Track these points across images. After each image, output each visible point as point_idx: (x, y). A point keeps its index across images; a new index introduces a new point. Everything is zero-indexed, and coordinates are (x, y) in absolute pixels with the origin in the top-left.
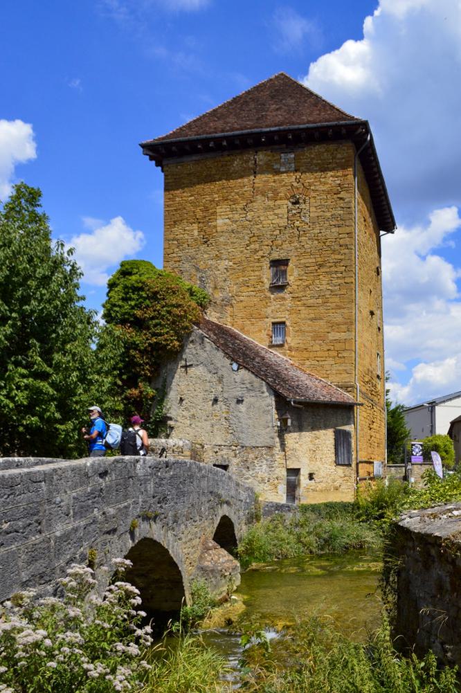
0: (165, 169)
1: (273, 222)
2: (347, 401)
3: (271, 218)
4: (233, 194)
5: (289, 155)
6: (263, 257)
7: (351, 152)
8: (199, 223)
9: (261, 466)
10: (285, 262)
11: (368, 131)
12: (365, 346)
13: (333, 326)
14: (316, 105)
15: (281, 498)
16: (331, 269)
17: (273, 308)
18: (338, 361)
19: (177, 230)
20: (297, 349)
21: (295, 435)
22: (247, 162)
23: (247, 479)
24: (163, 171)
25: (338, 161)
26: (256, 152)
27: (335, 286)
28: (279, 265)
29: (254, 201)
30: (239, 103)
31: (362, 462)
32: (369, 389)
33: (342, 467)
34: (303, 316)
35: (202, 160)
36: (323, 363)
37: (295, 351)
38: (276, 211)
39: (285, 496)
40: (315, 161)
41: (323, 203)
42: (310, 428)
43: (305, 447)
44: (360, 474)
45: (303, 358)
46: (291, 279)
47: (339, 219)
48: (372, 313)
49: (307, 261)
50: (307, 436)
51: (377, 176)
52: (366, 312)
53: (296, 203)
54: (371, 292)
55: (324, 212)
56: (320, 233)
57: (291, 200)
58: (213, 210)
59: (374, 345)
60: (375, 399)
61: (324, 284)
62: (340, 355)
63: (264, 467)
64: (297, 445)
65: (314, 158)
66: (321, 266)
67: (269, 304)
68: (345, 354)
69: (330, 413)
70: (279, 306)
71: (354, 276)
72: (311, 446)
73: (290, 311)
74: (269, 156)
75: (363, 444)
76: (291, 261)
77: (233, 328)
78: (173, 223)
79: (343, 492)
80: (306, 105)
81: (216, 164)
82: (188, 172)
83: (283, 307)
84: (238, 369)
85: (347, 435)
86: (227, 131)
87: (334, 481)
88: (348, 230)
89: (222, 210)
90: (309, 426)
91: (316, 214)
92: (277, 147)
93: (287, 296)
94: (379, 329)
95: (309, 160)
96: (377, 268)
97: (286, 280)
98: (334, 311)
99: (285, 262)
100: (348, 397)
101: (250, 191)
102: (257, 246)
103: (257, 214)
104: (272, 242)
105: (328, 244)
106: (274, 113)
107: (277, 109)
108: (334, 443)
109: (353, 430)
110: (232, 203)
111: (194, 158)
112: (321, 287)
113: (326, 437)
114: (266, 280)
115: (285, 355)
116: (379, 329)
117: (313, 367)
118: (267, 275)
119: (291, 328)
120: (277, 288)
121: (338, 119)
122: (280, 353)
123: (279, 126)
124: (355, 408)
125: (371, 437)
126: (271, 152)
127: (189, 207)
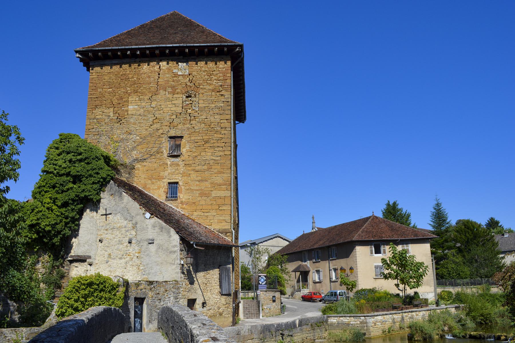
1: (172, 109)
6: (162, 134)
9: (169, 298)
17: (170, 171)
29: (158, 94)
36: (207, 214)
38: (173, 102)
46: (184, 150)
49: (196, 138)
51: (242, 82)
57: (186, 95)
62: (220, 208)
63: (172, 298)
66: (206, 142)
73: (183, 174)
79: (225, 317)
87: (219, 308)
91: (204, 105)
92: (176, 57)
98: (216, 175)
110: (140, 95)
114: (165, 151)
118: (166, 147)
119: (183, 187)
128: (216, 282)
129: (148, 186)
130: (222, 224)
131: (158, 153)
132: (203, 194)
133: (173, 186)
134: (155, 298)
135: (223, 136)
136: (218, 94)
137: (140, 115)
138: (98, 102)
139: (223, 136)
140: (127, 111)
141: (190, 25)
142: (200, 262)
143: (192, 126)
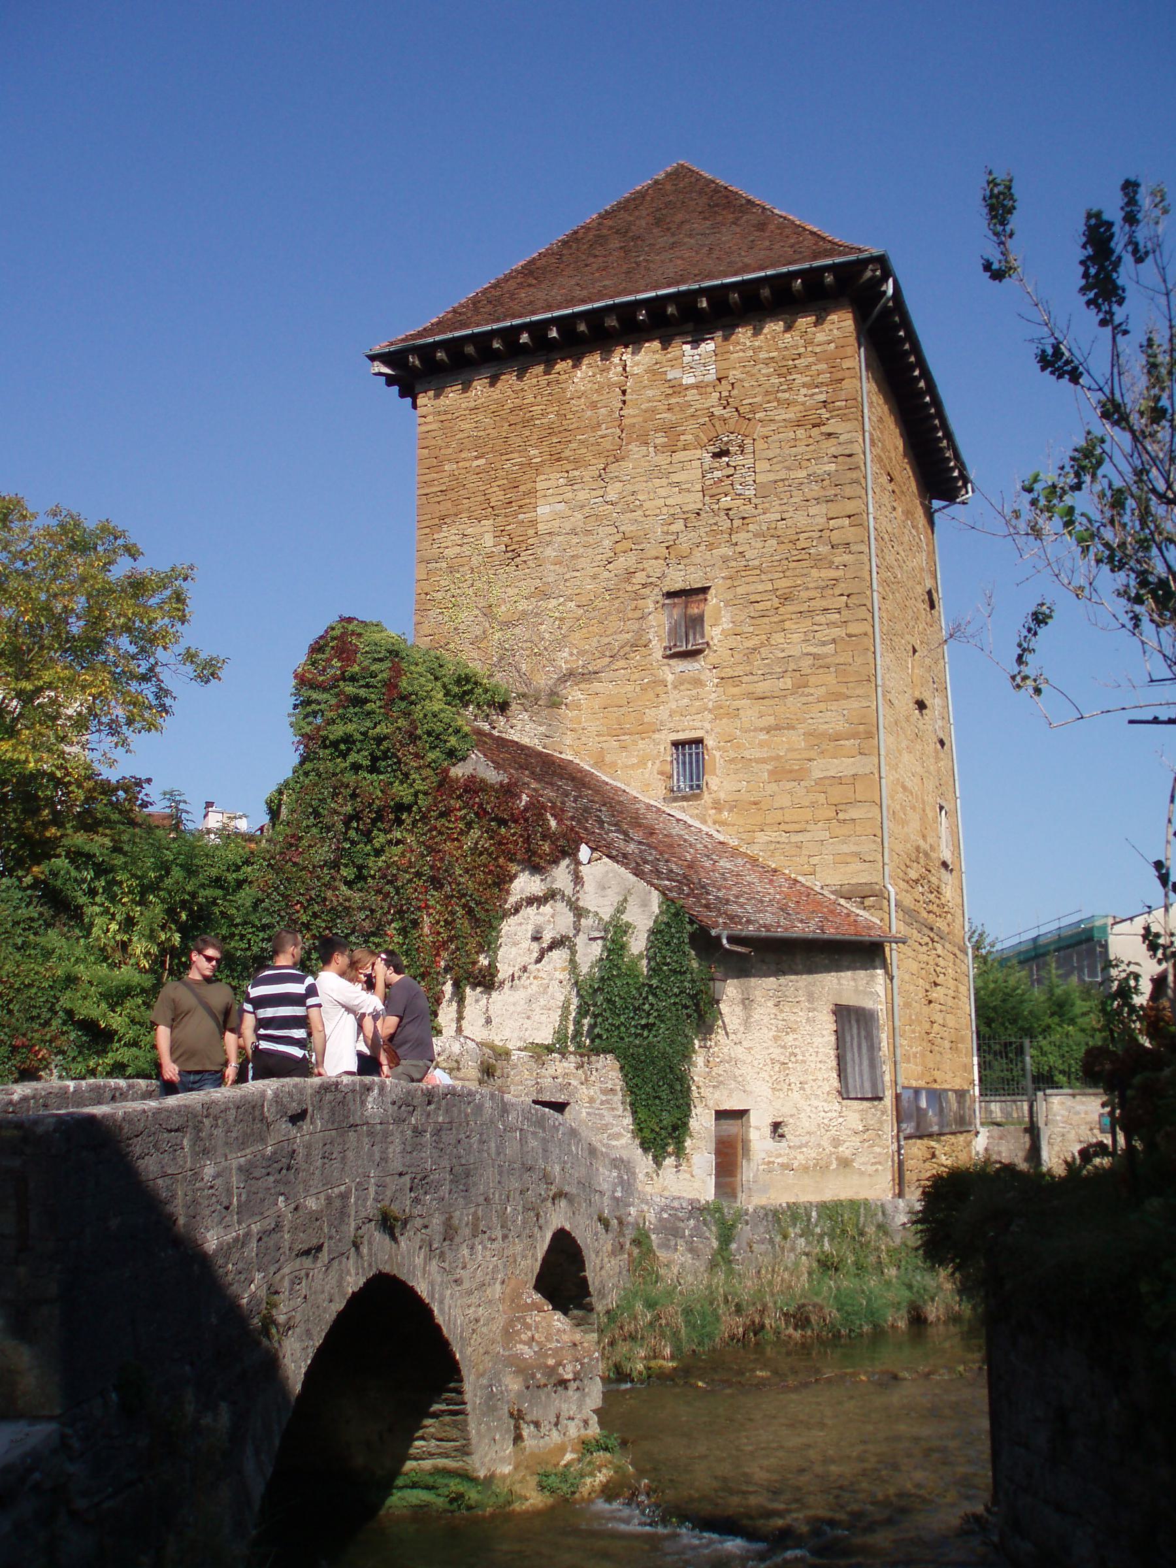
1: (670, 501)
3: (662, 492)
4: (573, 445)
6: (644, 586)
12: (905, 788)
14: (761, 227)
25: (818, 350)
27: (824, 644)
30: (578, 247)
32: (921, 898)
38: (675, 478)
40: (763, 355)
46: (714, 633)
49: (751, 588)
54: (915, 651)
58: (530, 485)
61: (793, 641)
62: (841, 816)
64: (739, 1049)
66: (786, 599)
68: (854, 813)
72: (776, 1052)
73: (720, 712)
77: (577, 761)
79: (862, 1173)
82: (472, 404)
88: (851, 507)
91: (772, 477)
97: (703, 637)
98: (822, 706)
104: (667, 548)
107: (673, 246)
118: (659, 624)
119: (717, 754)
124: (887, 949)
129: (608, 758)
135: (840, 573)
136: (815, 432)
140: (533, 523)
141: (722, 203)
143: (739, 549)
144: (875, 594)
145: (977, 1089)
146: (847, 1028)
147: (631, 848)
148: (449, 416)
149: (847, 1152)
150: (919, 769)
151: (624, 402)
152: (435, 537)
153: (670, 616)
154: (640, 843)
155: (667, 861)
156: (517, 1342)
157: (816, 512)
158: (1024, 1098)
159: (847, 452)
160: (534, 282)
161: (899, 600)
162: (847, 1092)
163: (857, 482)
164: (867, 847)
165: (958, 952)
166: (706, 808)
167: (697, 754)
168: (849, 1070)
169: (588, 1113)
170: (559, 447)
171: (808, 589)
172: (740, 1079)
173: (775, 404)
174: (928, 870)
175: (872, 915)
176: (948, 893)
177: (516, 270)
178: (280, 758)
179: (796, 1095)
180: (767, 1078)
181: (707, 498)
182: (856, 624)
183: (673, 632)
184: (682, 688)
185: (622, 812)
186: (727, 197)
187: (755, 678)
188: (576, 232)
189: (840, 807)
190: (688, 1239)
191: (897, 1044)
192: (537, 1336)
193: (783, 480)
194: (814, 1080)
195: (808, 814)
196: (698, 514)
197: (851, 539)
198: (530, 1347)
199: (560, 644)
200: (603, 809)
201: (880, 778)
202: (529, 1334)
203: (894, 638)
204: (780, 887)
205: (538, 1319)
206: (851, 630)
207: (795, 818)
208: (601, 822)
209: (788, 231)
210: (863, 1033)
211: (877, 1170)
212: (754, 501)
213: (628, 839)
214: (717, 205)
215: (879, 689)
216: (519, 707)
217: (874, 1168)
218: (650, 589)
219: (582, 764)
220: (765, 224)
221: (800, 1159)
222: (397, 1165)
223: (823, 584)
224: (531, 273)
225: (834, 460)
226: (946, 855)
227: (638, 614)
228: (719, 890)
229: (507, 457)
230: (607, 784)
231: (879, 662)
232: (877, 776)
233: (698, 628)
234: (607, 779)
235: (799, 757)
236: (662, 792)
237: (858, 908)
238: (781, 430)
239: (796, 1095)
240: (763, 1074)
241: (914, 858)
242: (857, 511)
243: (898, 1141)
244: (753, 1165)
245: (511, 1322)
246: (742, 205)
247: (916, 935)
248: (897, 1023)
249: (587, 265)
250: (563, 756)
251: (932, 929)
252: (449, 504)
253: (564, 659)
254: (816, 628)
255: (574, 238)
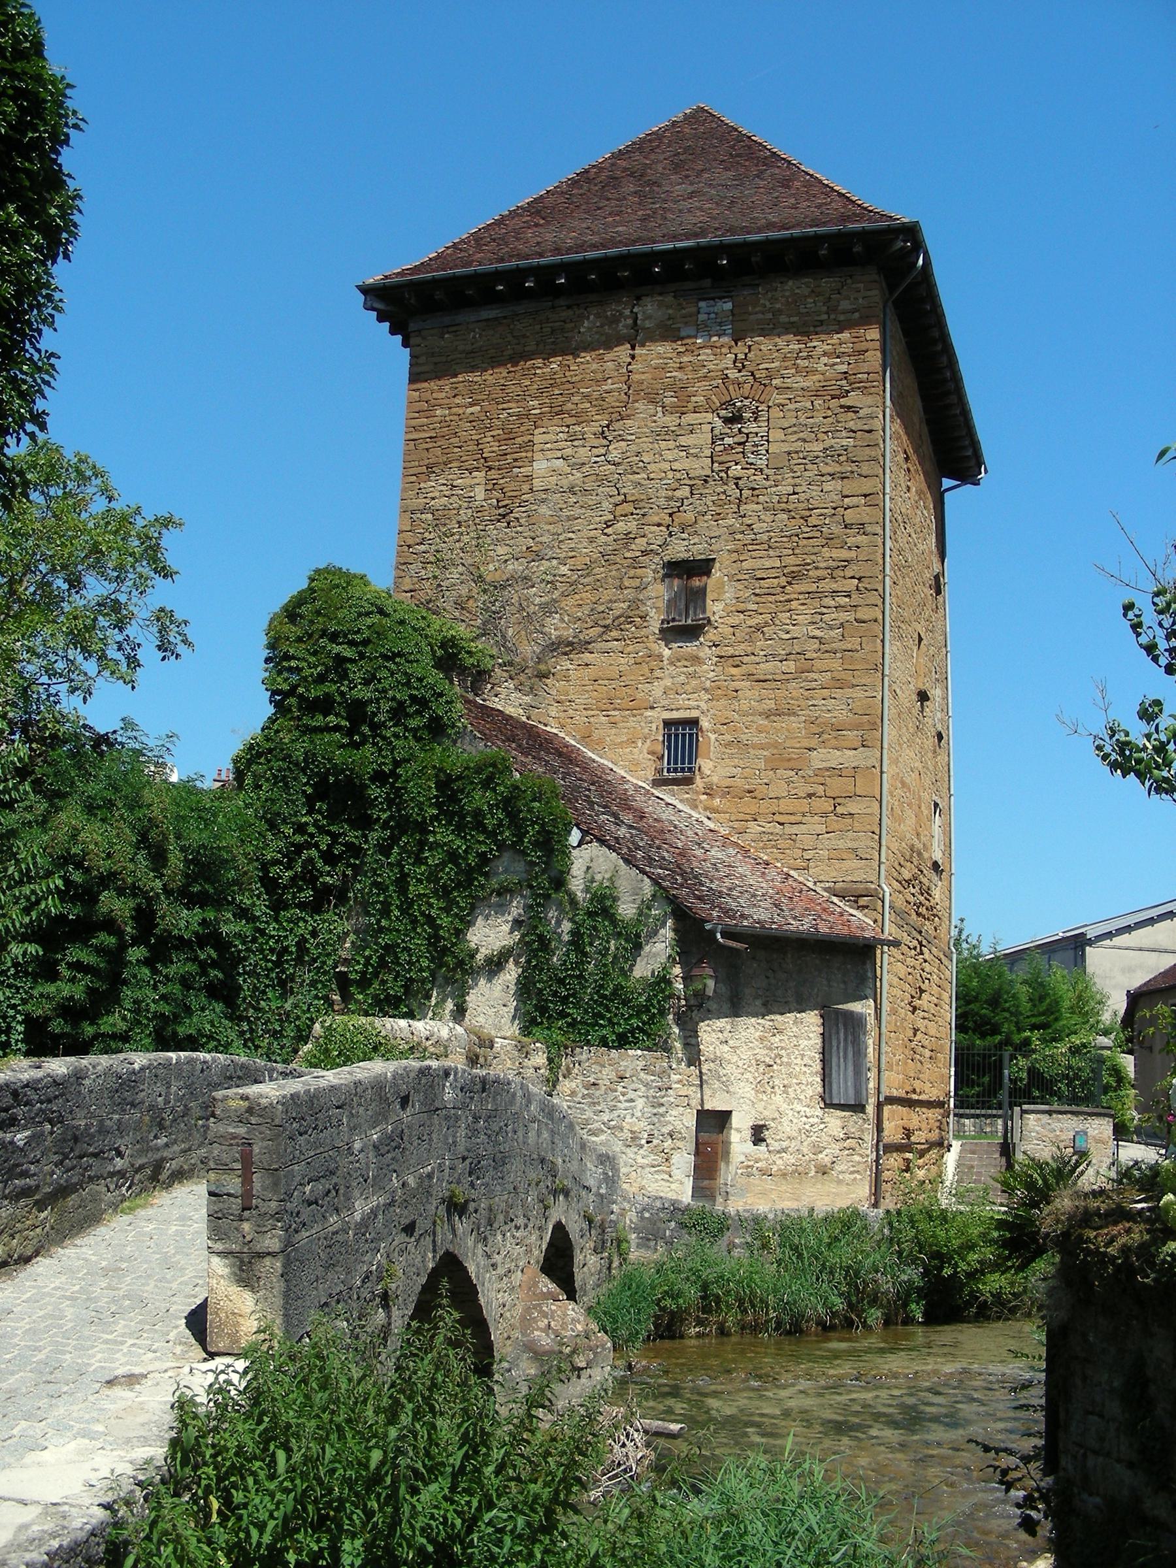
0: (413, 341)
1: (676, 466)
2: (859, 933)
3: (669, 456)
4: (576, 399)
5: (720, 303)
6: (645, 553)
7: (875, 294)
8: (490, 468)
9: (632, 1100)
10: (703, 567)
11: (918, 245)
12: (903, 784)
13: (826, 732)
14: (786, 183)
15: (679, 1186)
16: (822, 584)
17: (668, 682)
18: (835, 826)
19: (434, 486)
20: (727, 792)
21: (722, 1023)
22: (615, 320)
23: (594, 1133)
24: (405, 344)
25: (842, 318)
26: (638, 298)
27: (831, 628)
28: (689, 572)
29: (629, 417)
30: (593, 186)
31: (891, 1100)
32: (912, 899)
33: (839, 1113)
34: (745, 705)
35: (505, 318)
36: (795, 829)
37: (722, 797)
38: (683, 441)
39: (689, 1184)
40: (783, 319)
41: (802, 420)
42: (758, 1002)
43: (746, 1054)
44: (886, 1133)
45: (741, 816)
46: (715, 609)
47: (842, 458)
48: (923, 697)
49: (758, 563)
50: (751, 1028)
51: (939, 347)
52: (908, 697)
53: (734, 419)
54: (920, 639)
55: (804, 441)
56: (794, 493)
57: (723, 413)
58: (526, 439)
59: (927, 782)
60: (928, 927)
61: (801, 623)
62: (839, 810)
63: (640, 1103)
64: (726, 1048)
65: (780, 311)
66: (793, 577)
67: (658, 673)
68: (853, 807)
69: (812, 968)
70: (683, 677)
71: (880, 603)
72: (762, 1053)
73: (714, 692)
74: (668, 307)
75: (893, 1053)
76: (717, 565)
77: (562, 735)
78: (424, 469)
79: (839, 1182)
80: (762, 183)
81: (538, 327)
82: (469, 348)
83: (694, 682)
84: (579, 846)
85: (854, 1023)
86: (569, 250)
87: (818, 1149)
88: (867, 486)
89: (546, 437)
90: (757, 997)
91: (786, 447)
92: (689, 285)
93: (705, 653)
94: (940, 736)
95: (770, 316)
96: (937, 578)
97: (704, 612)
98: (826, 692)
99: (703, 567)
100: (861, 922)
101: (619, 390)
102: (632, 526)
103: (634, 448)
104: (671, 515)
105: (813, 521)
106: (685, 205)
107: (691, 195)
108: (820, 1045)
109: (872, 1012)
110: (573, 420)
111: (486, 314)
112: (796, 631)
113: (803, 1031)
114: (652, 613)
115: (695, 807)
116: (940, 736)
117: (769, 841)
118: (658, 596)
119: (713, 737)
120: (684, 630)
121: (844, 219)
122: (681, 801)
123: (696, 235)
124: (878, 952)
125: (916, 1031)
126: (675, 297)
127: (467, 432)
128: (806, 1060)
129: (596, 735)
130: (847, 864)
131: (629, 620)
132: (780, 760)
133: (682, 738)
134: (583, 1097)
135: (853, 554)
136: (834, 403)
137: (572, 490)
138: (436, 455)
139: (853, 554)
140: (529, 478)
141: (747, 154)
142: (747, 991)
143: (747, 521)
144: (887, 579)
145: (952, 1100)
146: (833, 1031)
147: (622, 832)
148: (444, 359)
149: (827, 1159)
150: (918, 764)
151: (633, 357)
152: (422, 485)
153: (671, 587)
154: (631, 827)
155: (659, 848)
156: (534, 1329)
157: (831, 488)
158: (1000, 1112)
159: (866, 428)
160: (542, 222)
161: (909, 585)
162: (831, 1097)
163: (875, 460)
164: (865, 842)
165: (942, 957)
166: (697, 793)
167: (691, 735)
168: (834, 1075)
169: (569, 1107)
170: (561, 399)
171: (817, 568)
172: (724, 1079)
173: (793, 371)
174: (925, 874)
175: (865, 915)
176: (937, 893)
177: (521, 208)
178: (249, 711)
179: (778, 1099)
180: (751, 1080)
181: (716, 465)
182: (866, 609)
183: (672, 604)
184: (678, 664)
185: (610, 793)
186: (750, 147)
187: (757, 659)
188: (586, 171)
189: (838, 800)
190: (668, 1239)
191: (883, 1051)
192: (552, 1324)
193: (797, 452)
194: (798, 1084)
195: (804, 805)
196: (706, 481)
197: (866, 520)
198: (547, 1335)
199: (549, 609)
200: (592, 787)
201: (882, 772)
202: (546, 1321)
203: (902, 625)
204: (772, 881)
205: (553, 1307)
206: (860, 616)
207: (791, 809)
208: (592, 803)
209: (815, 190)
210: (850, 1037)
211: (855, 1179)
212: (766, 471)
213: (619, 823)
214: (738, 155)
215: (886, 679)
216: (505, 674)
217: (852, 1177)
218: (651, 556)
219: (567, 739)
220: (789, 180)
221: (780, 1163)
222: (461, 1149)
223: (835, 564)
224: (538, 212)
225: (853, 435)
226: (938, 856)
227: (637, 582)
228: (712, 881)
229: (505, 406)
230: (594, 761)
231: (887, 650)
232: (878, 769)
233: (700, 602)
234: (594, 756)
235: (798, 745)
236: (650, 775)
237: (851, 907)
238: (798, 399)
239: (778, 1099)
240: (748, 1075)
241: (908, 858)
242: (874, 490)
243: (877, 1151)
244: (732, 1168)
245: (527, 1310)
246: (766, 158)
247: (906, 939)
248: (884, 1030)
249: (599, 209)
250: (548, 729)
251: (920, 932)
252: (438, 451)
253: (556, 627)
254: (825, 610)
255: (584, 176)
